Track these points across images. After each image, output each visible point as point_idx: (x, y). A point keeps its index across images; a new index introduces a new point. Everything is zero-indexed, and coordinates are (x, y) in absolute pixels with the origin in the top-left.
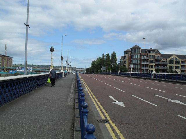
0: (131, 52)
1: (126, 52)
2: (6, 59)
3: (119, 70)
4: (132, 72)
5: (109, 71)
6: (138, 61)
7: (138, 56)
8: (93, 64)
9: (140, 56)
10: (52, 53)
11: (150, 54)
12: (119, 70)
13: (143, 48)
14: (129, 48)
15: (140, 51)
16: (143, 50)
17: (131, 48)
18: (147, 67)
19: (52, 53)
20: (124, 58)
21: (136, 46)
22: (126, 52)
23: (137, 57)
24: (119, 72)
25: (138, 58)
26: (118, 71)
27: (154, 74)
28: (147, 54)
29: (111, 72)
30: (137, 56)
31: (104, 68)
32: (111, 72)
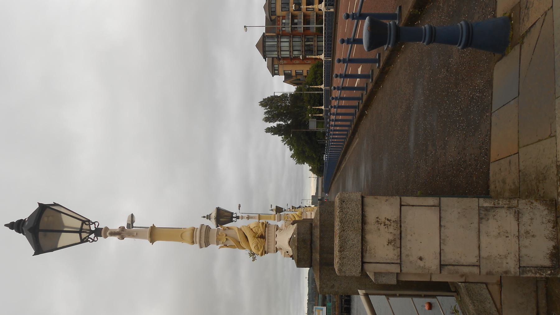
0: (273, 58)
1: (274, 72)
2: (292, 49)
3: (319, 87)
4: (322, 57)
5: (321, 111)
6: (297, 40)
7: (282, 40)
8: (301, 156)
9: (284, 35)
10: (238, 218)
11: (279, 12)
12: (319, 87)
13: (263, 30)
14: (262, 64)
15: (272, 37)
16: (267, 30)
17: (265, 57)
18: (311, 20)
19: (238, 218)
20: (288, 78)
21: (257, 46)
22: (274, 72)
23: (287, 44)
24: (322, 86)
25: (288, 40)
26: (321, 90)
27: (325, 5)
28: (279, 17)
29: (323, 107)
30: (283, 44)
31: (313, 125)
32: (323, 107)
